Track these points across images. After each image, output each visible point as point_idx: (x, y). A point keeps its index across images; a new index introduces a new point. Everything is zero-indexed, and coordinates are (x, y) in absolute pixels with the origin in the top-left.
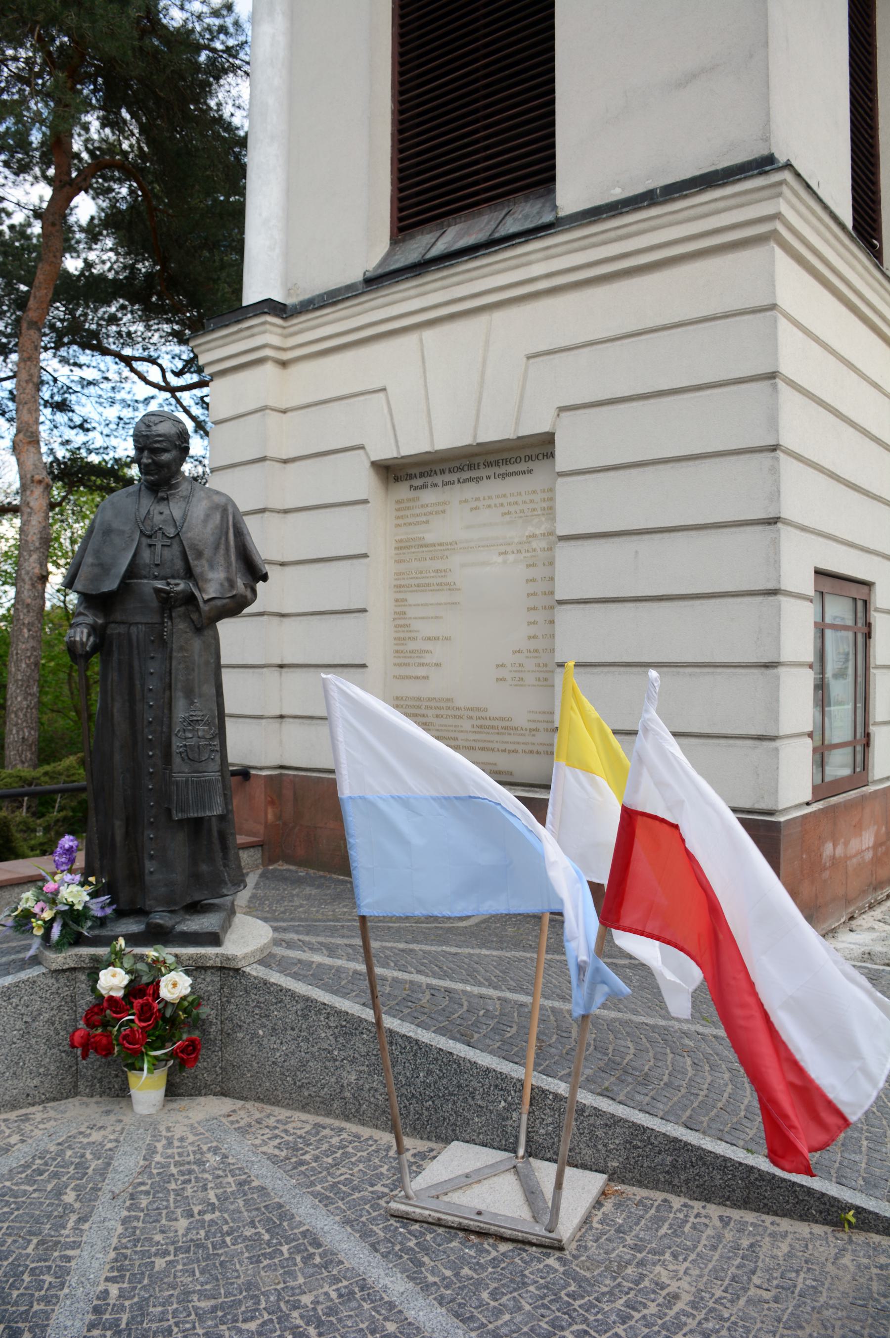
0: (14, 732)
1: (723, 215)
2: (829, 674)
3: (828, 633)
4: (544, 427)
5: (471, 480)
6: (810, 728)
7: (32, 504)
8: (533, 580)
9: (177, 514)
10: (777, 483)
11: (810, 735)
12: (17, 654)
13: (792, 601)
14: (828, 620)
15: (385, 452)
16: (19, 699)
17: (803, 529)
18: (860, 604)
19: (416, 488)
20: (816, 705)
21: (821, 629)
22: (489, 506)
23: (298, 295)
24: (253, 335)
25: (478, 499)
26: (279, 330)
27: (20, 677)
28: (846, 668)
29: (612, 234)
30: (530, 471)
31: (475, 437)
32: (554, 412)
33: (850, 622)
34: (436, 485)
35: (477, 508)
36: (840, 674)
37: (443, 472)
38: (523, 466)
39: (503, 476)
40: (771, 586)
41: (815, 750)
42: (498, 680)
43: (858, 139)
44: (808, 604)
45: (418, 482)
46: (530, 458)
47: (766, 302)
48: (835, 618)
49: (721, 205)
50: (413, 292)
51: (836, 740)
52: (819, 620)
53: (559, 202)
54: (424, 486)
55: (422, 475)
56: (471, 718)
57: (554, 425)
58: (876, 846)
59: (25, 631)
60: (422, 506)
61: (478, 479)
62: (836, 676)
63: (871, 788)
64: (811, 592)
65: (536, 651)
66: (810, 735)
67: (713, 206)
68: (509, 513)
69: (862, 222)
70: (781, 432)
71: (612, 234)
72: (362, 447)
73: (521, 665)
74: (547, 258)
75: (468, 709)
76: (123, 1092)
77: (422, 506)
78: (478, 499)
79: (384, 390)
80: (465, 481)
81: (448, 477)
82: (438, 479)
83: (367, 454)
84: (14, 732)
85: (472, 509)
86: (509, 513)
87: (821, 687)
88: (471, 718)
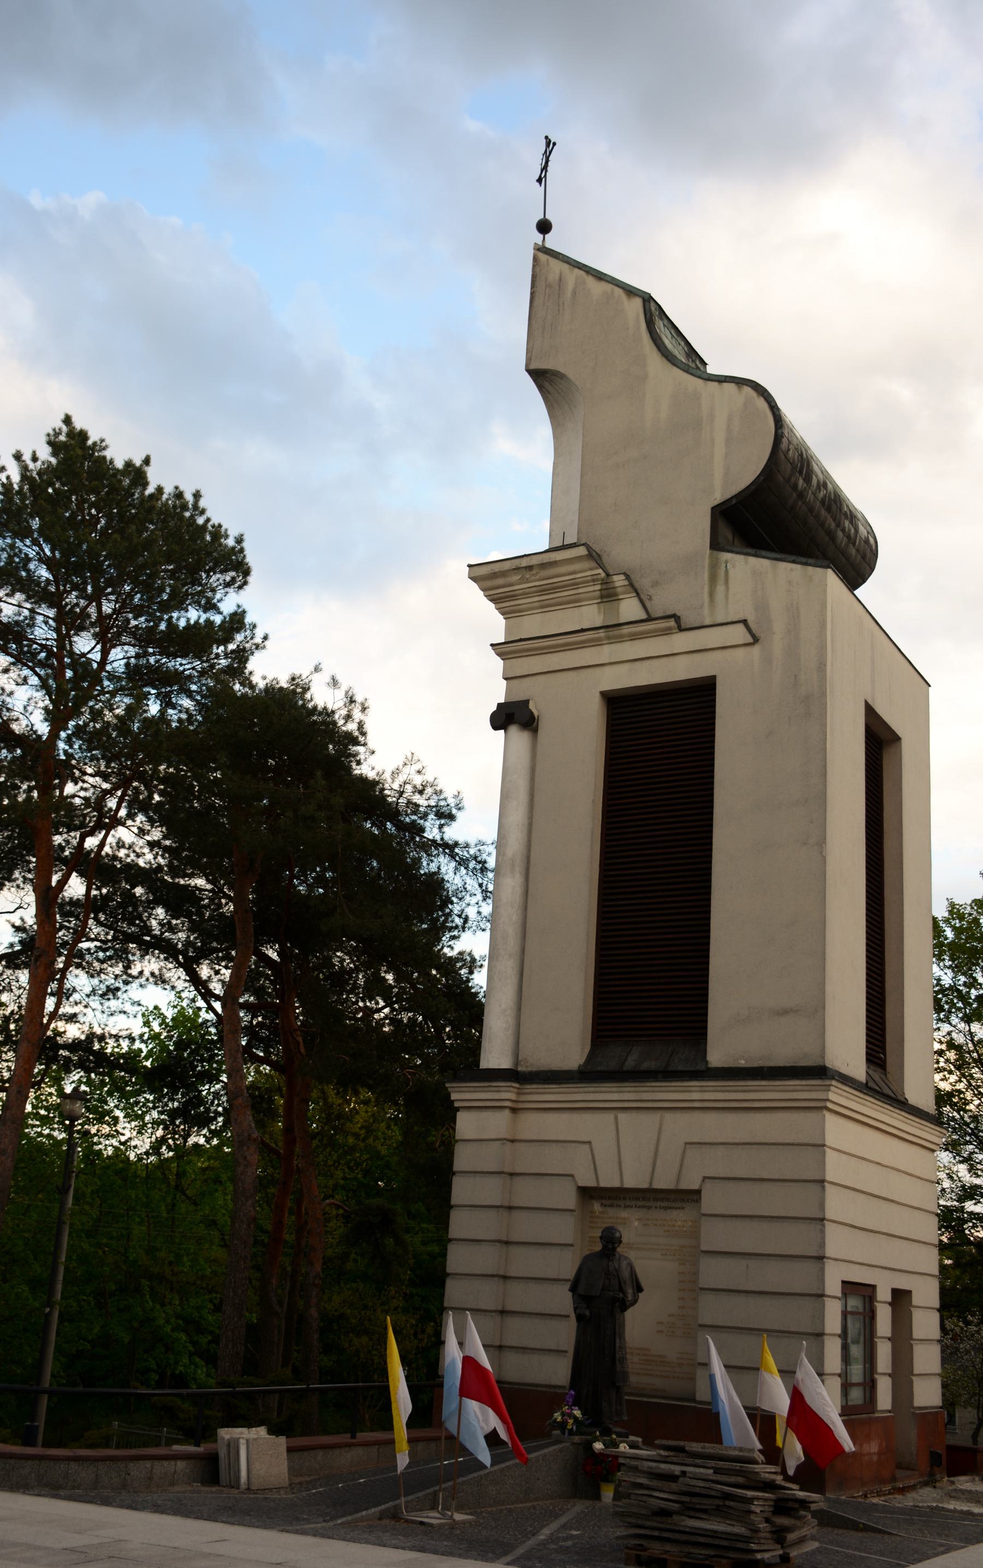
0: (230, 1347)
1: (800, 1093)
2: (849, 1341)
3: (849, 1317)
4: (695, 1186)
5: (644, 1207)
6: (839, 1371)
7: (248, 1158)
8: (683, 1273)
9: (617, 1266)
10: (823, 1238)
11: (839, 1375)
12: (235, 1282)
13: (830, 1299)
14: (849, 1309)
15: (588, 1181)
16: (236, 1319)
17: (836, 1260)
18: (867, 1299)
19: (605, 1206)
20: (842, 1360)
21: (845, 1314)
22: (656, 1225)
23: (527, 1067)
24: (499, 1091)
25: (648, 1219)
26: (516, 1090)
27: (237, 1301)
28: (859, 1338)
29: (740, 1088)
30: (683, 1208)
31: (651, 1184)
32: (700, 1179)
33: (861, 1310)
34: (620, 1206)
35: (647, 1225)
36: (856, 1342)
37: (625, 1199)
38: (679, 1204)
39: (666, 1208)
40: (819, 1292)
41: (842, 1385)
42: (658, 1332)
43: (871, 747)
44: (838, 1301)
45: (608, 1202)
46: (683, 1200)
47: (820, 1143)
48: (853, 1307)
49: (799, 1088)
50: (614, 1089)
51: (854, 1381)
52: (844, 1309)
53: (709, 1058)
54: (611, 1206)
55: (610, 1198)
56: (639, 1354)
57: (701, 1186)
58: (880, 1453)
59: (242, 1263)
60: (610, 1218)
61: (649, 1208)
62: (853, 1342)
63: (877, 1415)
64: (840, 1295)
65: (683, 1316)
66: (839, 1375)
67: (795, 1088)
68: (668, 1231)
69: (874, 876)
70: (826, 1211)
71: (740, 1088)
72: (572, 1176)
73: (673, 1324)
74: (701, 1091)
75: (637, 1349)
76: (597, 1496)
77: (610, 1218)
78: (648, 1219)
79: (589, 1142)
80: (639, 1207)
81: (628, 1203)
82: (621, 1203)
83: (575, 1181)
84: (230, 1347)
85: (644, 1225)
86: (668, 1231)
87: (845, 1347)
88: (639, 1354)
